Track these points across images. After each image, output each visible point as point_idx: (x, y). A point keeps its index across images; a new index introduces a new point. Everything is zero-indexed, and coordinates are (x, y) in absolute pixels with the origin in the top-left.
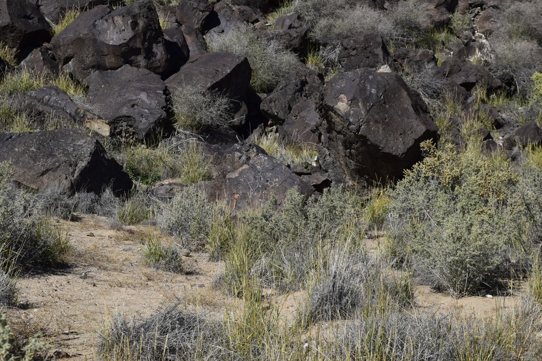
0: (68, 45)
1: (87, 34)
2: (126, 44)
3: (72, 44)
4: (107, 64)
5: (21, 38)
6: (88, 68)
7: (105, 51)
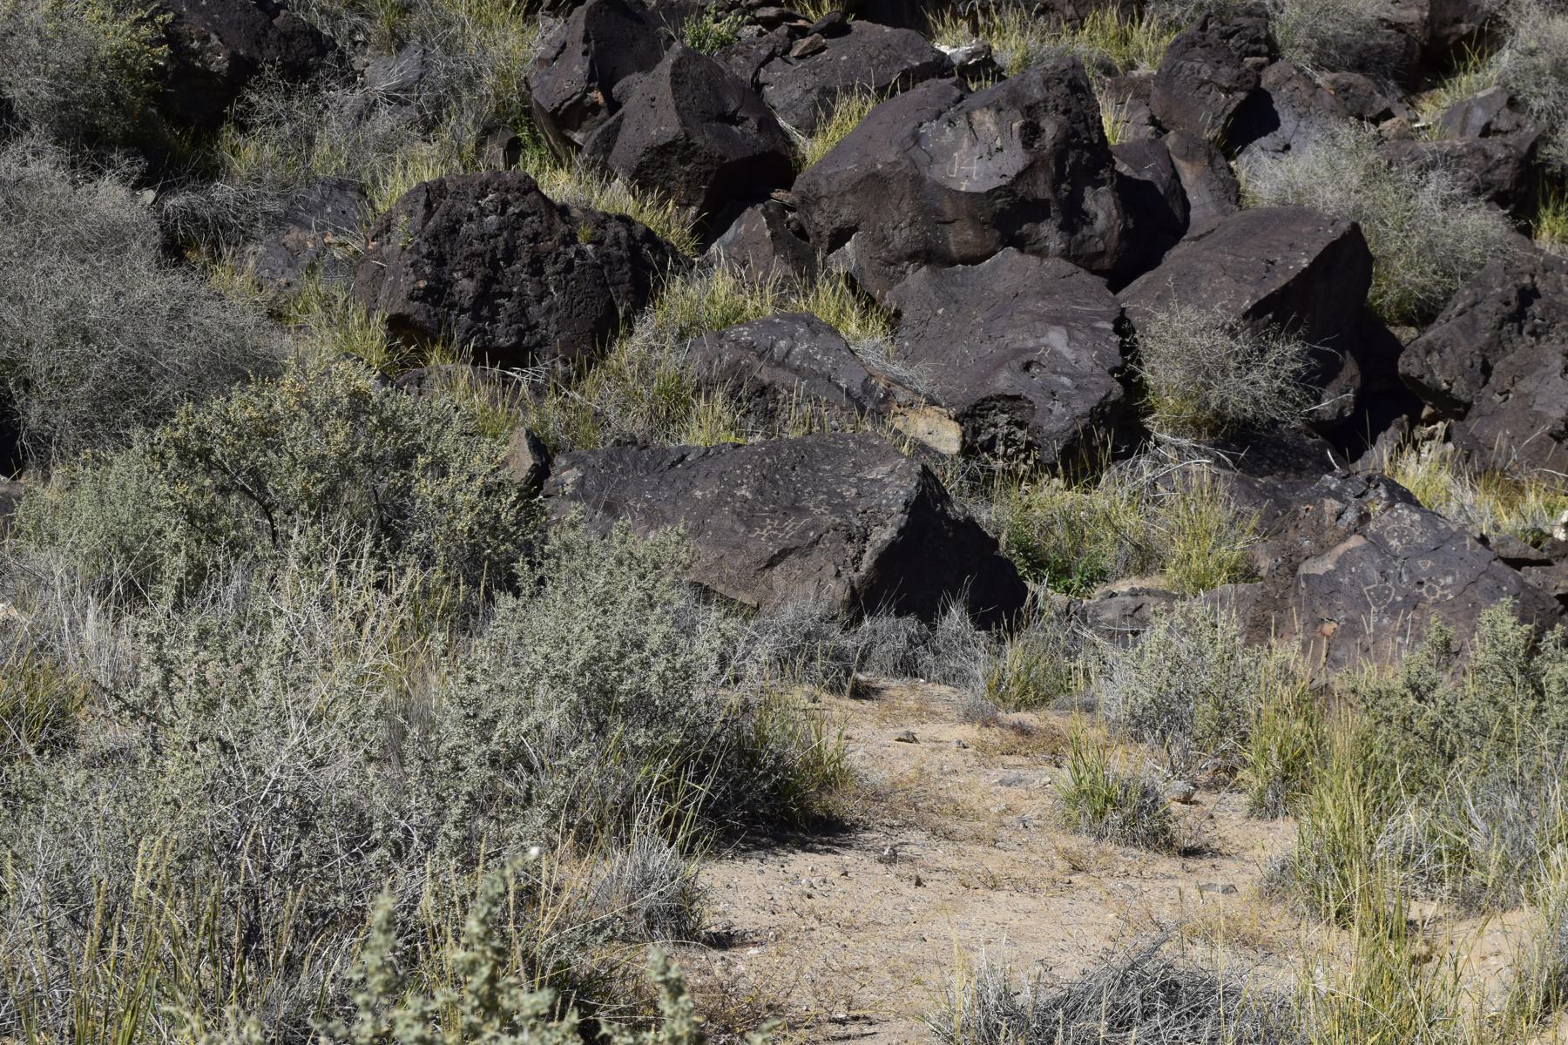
0: (843, 194)
1: (896, 163)
2: (1008, 190)
3: (854, 190)
4: (953, 248)
5: (711, 177)
6: (900, 260)
7: (948, 209)
